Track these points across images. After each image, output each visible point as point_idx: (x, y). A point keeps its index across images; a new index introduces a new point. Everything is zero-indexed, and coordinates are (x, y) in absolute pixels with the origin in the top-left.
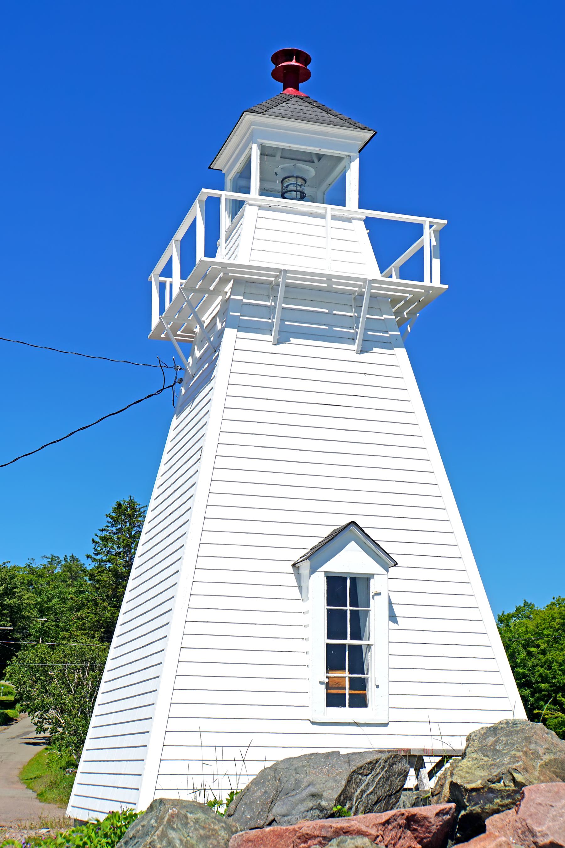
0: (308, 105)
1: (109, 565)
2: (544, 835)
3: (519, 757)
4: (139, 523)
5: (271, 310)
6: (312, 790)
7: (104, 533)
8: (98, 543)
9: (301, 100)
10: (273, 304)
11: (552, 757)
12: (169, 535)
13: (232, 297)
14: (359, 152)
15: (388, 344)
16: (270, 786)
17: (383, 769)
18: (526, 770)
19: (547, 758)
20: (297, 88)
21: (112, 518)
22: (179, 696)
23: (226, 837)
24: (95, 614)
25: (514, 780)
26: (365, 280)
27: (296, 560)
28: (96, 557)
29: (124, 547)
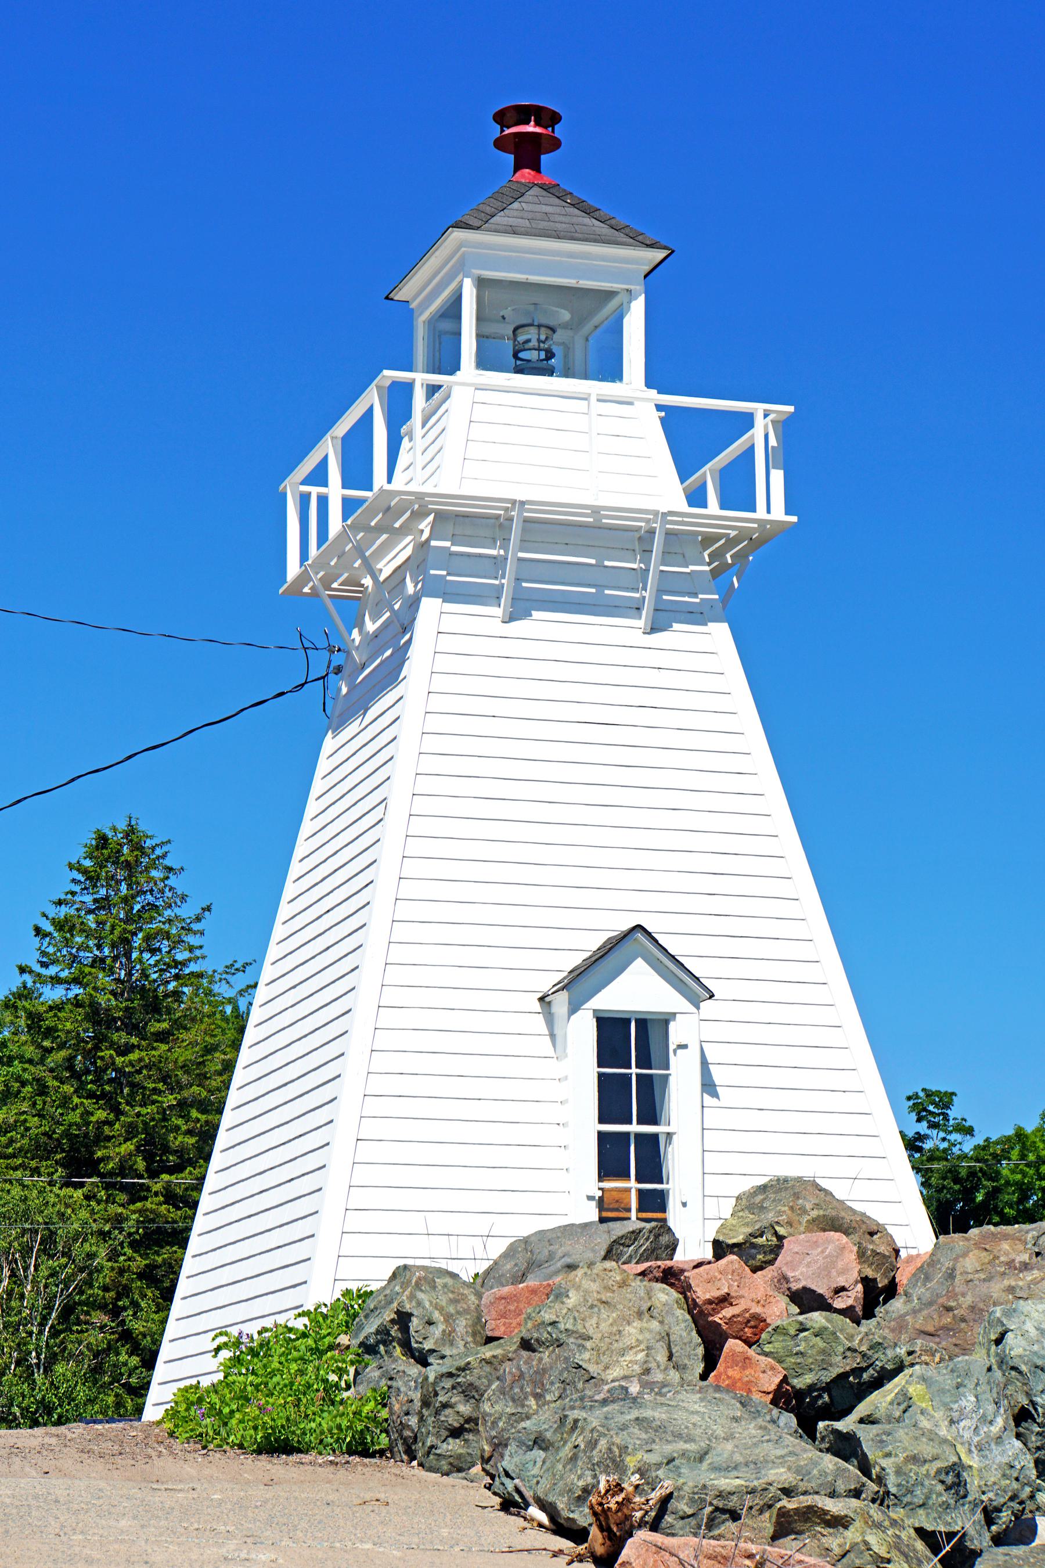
0: (557, 201)
1: (77, 990)
2: (797, 1280)
3: (784, 1212)
4: (151, 884)
5: (498, 563)
6: (568, 1260)
7: (64, 911)
8: (46, 935)
9: (544, 193)
10: (502, 552)
11: (821, 1213)
12: (328, 948)
13: (433, 543)
14: (645, 277)
15: (697, 616)
16: (522, 1260)
17: (647, 1239)
18: (790, 1224)
19: (814, 1213)
20: (536, 168)
21: (85, 872)
22: (355, 1220)
23: (477, 1302)
24: (40, 1115)
25: (776, 1233)
26: (656, 513)
27: (545, 990)
28: (43, 971)
29: (113, 946)
